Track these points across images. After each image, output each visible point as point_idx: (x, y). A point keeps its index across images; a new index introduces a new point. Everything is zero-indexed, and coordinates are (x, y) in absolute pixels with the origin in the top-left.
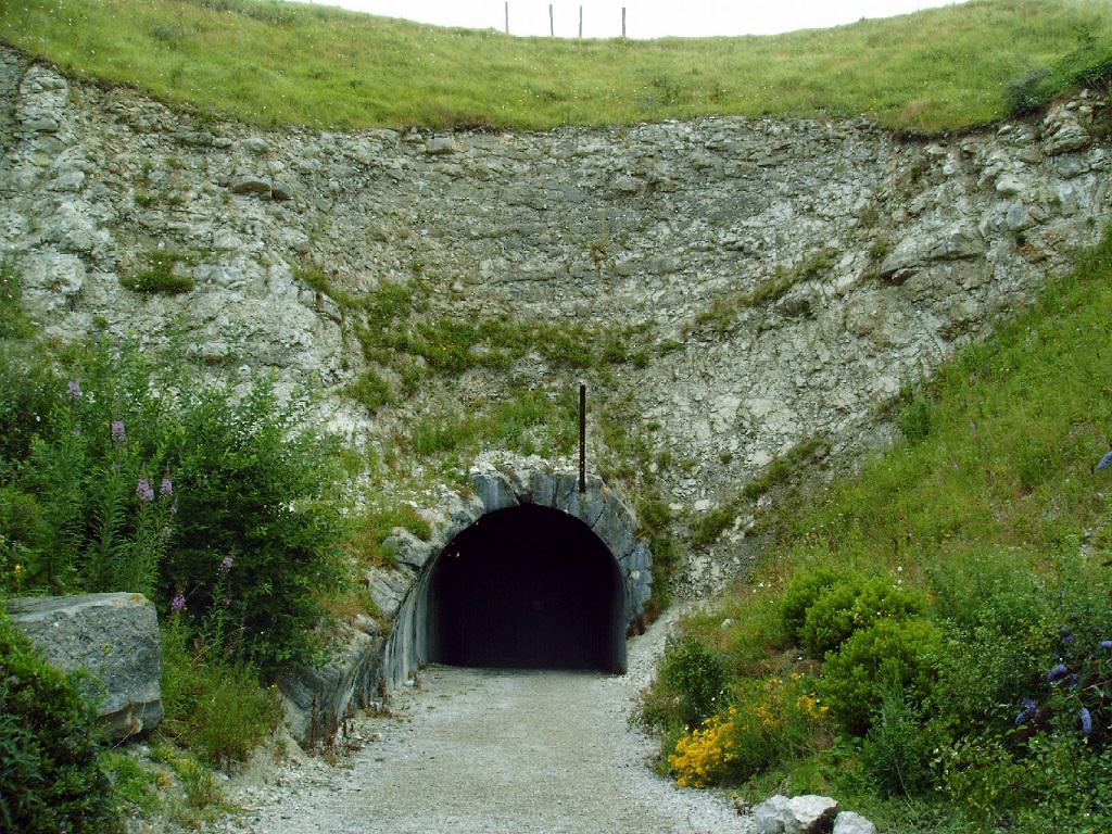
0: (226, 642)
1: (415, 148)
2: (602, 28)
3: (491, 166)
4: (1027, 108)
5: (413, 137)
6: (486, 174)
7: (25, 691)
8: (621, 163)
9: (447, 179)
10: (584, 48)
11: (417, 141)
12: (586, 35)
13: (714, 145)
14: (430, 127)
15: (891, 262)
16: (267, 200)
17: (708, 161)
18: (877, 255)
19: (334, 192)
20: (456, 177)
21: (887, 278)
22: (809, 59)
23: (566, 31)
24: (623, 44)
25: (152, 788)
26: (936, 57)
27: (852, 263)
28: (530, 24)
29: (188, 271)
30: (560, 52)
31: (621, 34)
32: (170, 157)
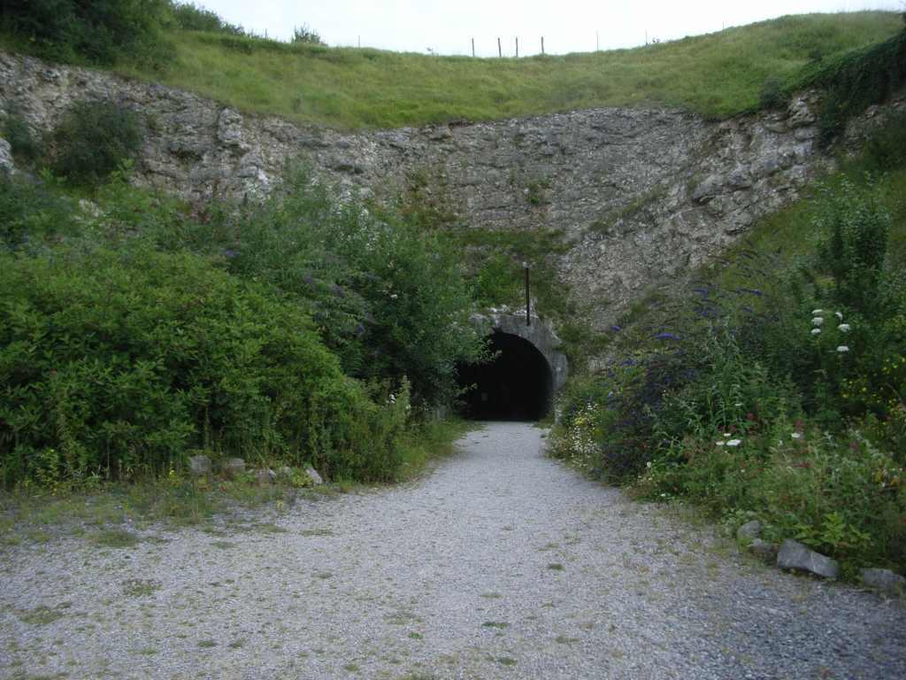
0: (214, 316)
1: (428, 136)
2: (529, 50)
3: (471, 143)
4: (774, 103)
5: (426, 131)
6: (468, 148)
7: (65, 101)
8: (544, 138)
9: (446, 152)
10: (520, 64)
11: (429, 132)
12: (521, 55)
13: (597, 125)
14: (436, 122)
15: (698, 192)
16: (352, 174)
17: (595, 135)
18: (691, 188)
19: (385, 165)
20: (451, 151)
21: (697, 202)
22: (656, 65)
23: (509, 53)
24: (542, 59)
25: (22, 112)
26: (726, 65)
27: (676, 194)
28: (486, 51)
29: (190, 395)
30: (502, 68)
31: (541, 52)
32: (299, 153)
